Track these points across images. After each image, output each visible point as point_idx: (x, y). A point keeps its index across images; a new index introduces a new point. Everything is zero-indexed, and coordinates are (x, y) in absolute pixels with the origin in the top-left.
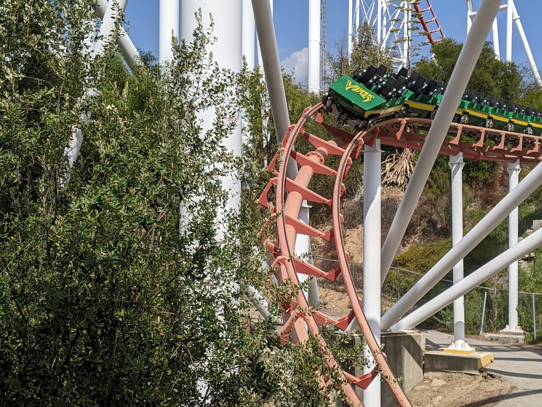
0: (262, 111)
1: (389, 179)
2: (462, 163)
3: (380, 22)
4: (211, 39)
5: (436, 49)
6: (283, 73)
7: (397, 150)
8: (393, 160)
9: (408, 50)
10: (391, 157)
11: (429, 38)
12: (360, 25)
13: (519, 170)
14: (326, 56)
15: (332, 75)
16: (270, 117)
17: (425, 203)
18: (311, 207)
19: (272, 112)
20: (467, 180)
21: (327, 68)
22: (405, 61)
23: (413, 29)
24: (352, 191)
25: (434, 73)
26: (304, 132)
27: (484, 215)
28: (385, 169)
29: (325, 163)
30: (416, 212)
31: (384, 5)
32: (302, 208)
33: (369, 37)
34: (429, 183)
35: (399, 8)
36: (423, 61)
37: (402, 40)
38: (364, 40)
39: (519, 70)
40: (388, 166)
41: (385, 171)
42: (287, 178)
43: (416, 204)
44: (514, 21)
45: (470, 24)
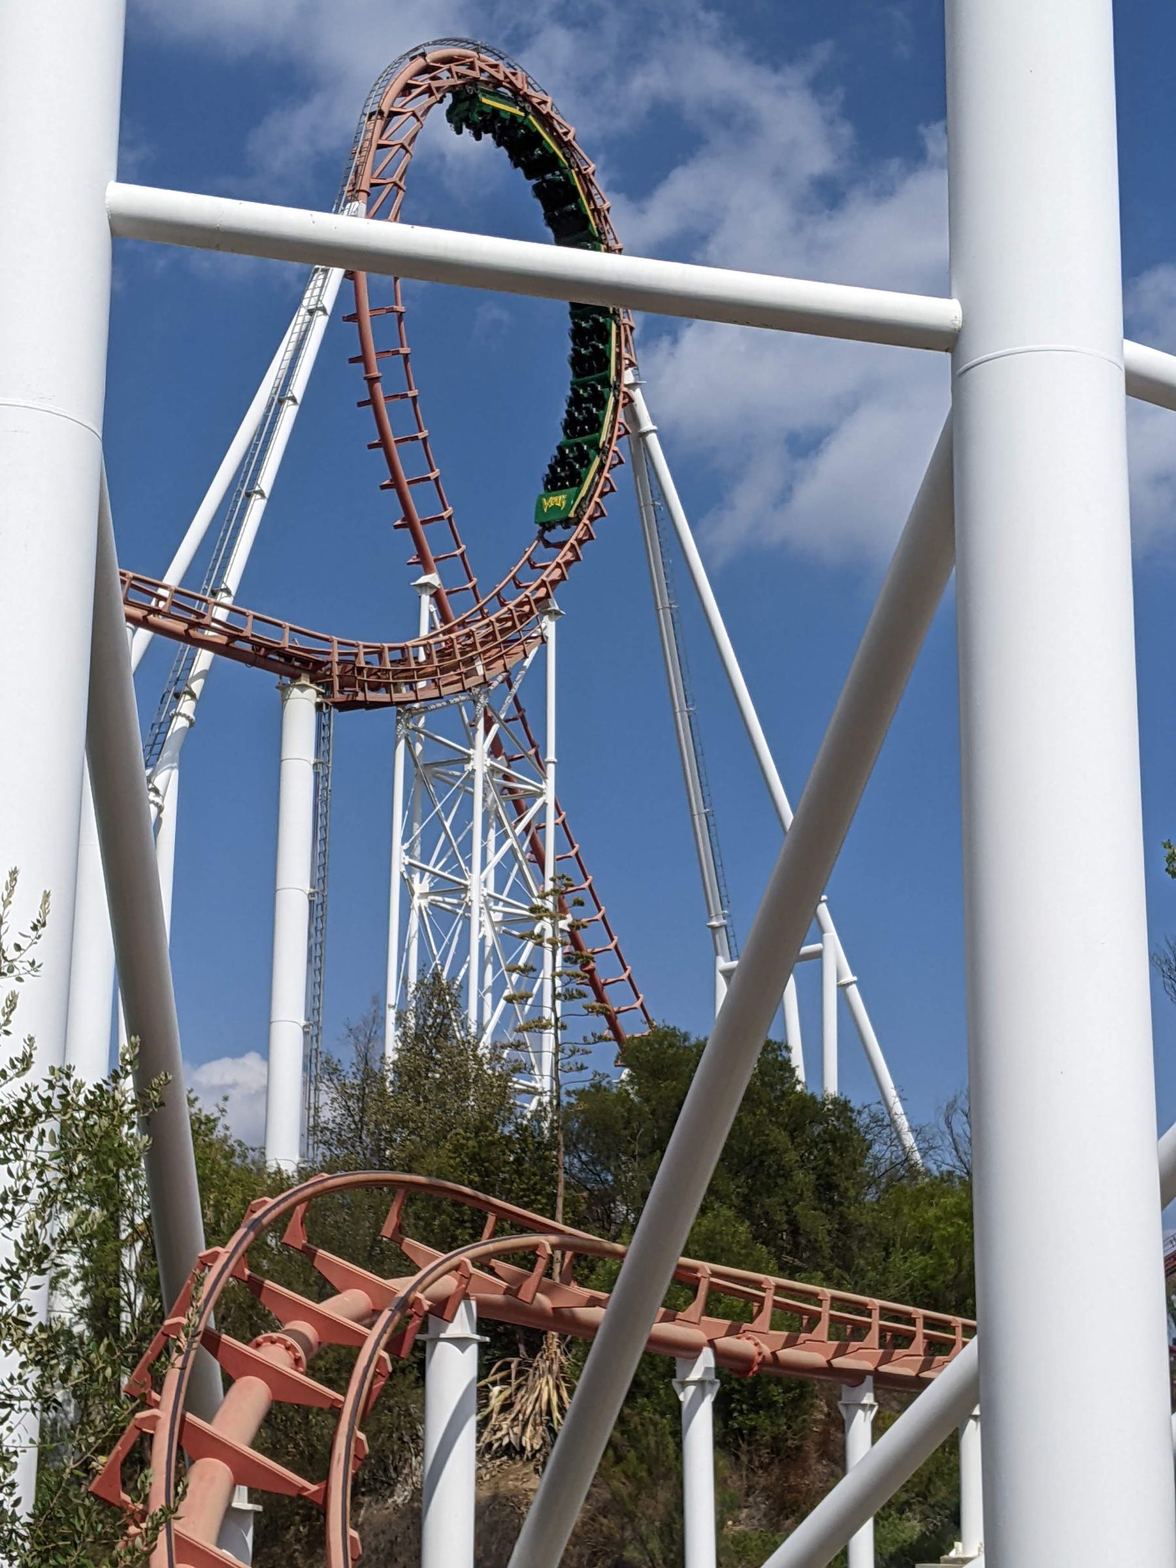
0: (124, 1223)
1: (499, 1435)
2: (712, 1383)
3: (476, 977)
4: (21, 967)
5: (630, 1054)
6: (194, 1110)
7: (522, 1348)
8: (509, 1377)
9: (555, 1054)
10: (507, 1366)
11: (613, 1026)
12: (420, 983)
13: (872, 1406)
14: (318, 1067)
15: (338, 1120)
16: (145, 1242)
17: (604, 1511)
18: (259, 1508)
19: (154, 1228)
20: (726, 1441)
21: (324, 1098)
22: (545, 1084)
23: (568, 996)
24: (386, 1470)
25: (628, 1123)
26: (247, 1272)
27: (776, 1546)
28: (486, 1405)
29: (309, 1367)
30: (576, 1538)
31: (488, 931)
32: (231, 1513)
33: (446, 1015)
34: (615, 1449)
35: (531, 936)
36: (597, 1087)
37: (537, 1025)
38: (430, 1022)
39: (863, 1120)
40: (497, 1395)
41: (489, 1410)
42: (189, 1416)
43: (576, 1515)
44: (842, 988)
45: (722, 989)
